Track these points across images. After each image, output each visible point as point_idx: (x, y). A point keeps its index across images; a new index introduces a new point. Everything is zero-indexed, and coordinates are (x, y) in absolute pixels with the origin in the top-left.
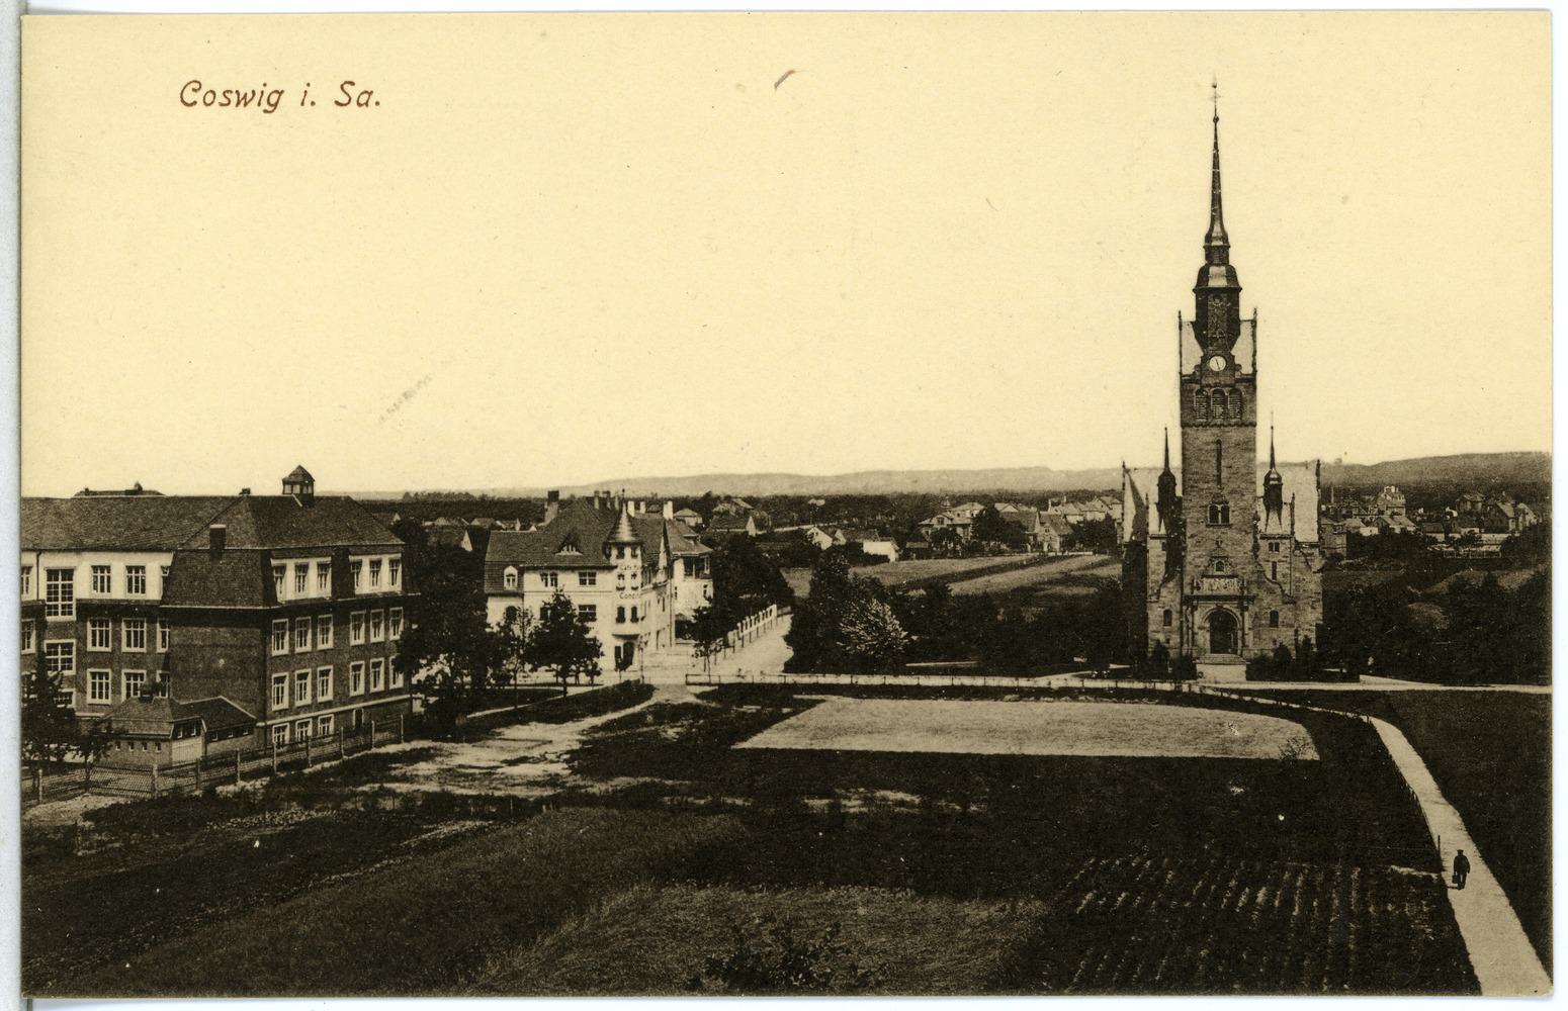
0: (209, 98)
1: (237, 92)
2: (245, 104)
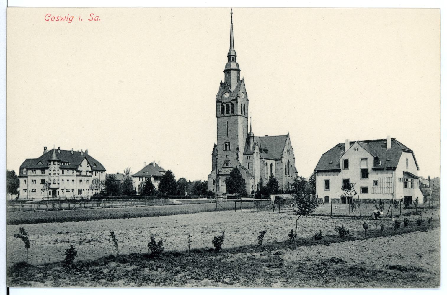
0: (53, 19)
1: (61, 17)
2: (63, 20)
